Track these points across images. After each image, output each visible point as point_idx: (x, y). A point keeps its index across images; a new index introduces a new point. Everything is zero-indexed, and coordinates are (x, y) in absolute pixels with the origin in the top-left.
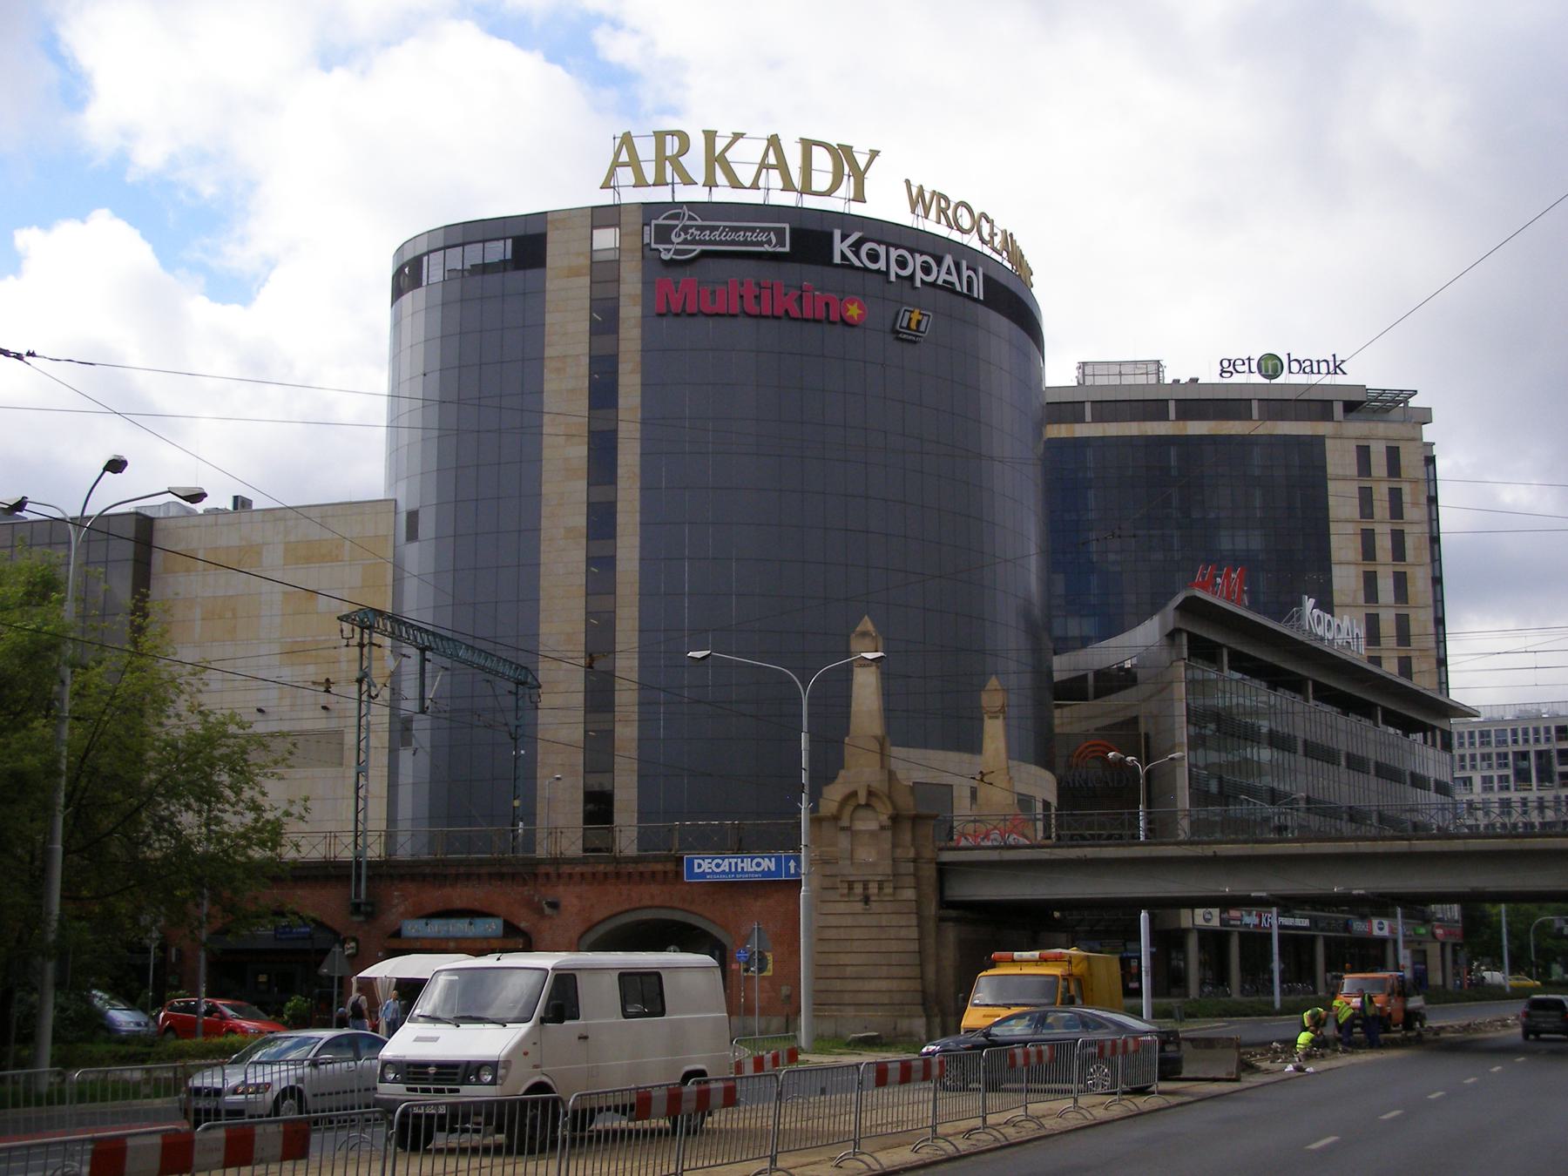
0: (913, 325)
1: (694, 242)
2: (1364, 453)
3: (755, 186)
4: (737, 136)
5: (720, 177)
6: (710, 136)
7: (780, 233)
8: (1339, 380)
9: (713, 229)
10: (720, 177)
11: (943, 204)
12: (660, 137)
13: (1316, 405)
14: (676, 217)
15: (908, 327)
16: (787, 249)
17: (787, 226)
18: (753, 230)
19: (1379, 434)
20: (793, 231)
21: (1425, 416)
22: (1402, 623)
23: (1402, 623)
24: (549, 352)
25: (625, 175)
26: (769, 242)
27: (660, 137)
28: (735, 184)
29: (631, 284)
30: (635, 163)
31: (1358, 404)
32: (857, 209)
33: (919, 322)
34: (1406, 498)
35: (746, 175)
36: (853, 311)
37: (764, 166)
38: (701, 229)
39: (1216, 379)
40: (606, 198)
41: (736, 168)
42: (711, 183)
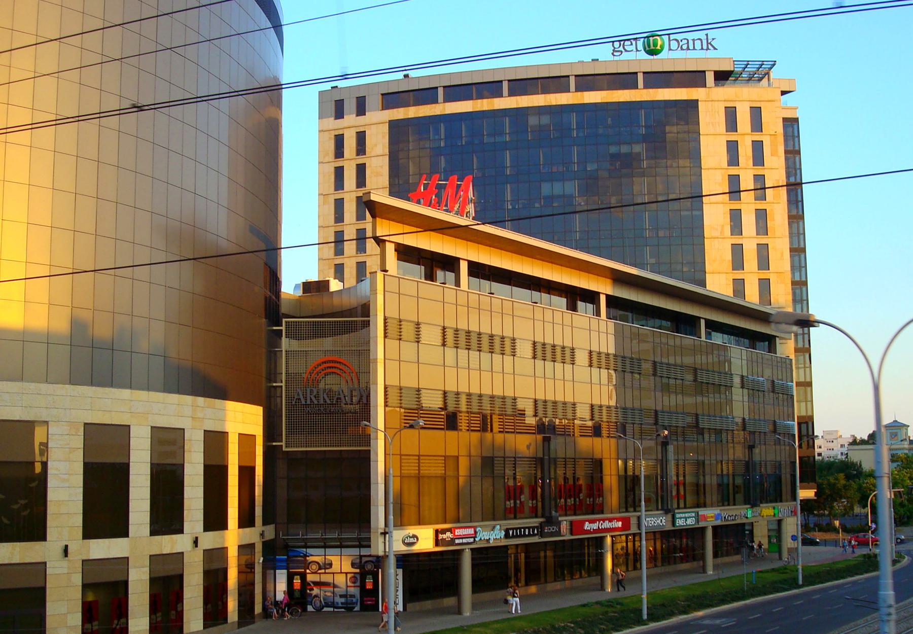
2: (731, 115)
16: (284, 320)
39: (611, 58)
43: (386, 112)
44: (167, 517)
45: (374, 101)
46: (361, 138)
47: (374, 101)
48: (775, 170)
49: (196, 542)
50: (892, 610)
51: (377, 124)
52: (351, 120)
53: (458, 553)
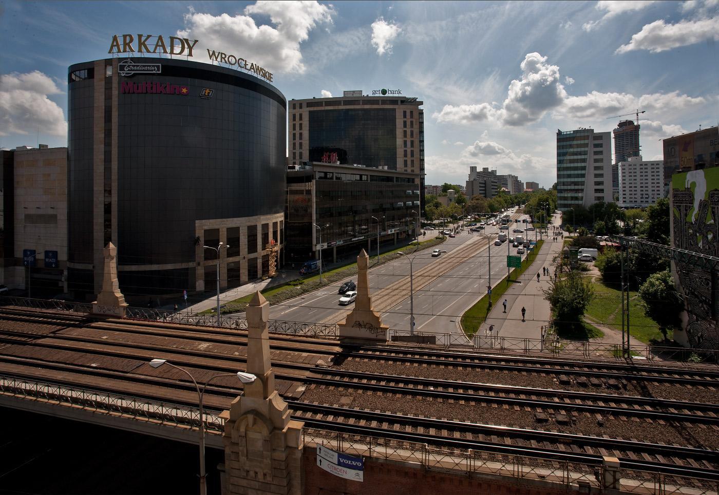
0: (206, 94)
1: (131, 70)
2: (405, 112)
3: (154, 52)
4: (149, 36)
5: (143, 49)
6: (140, 36)
7: (158, 67)
8: (400, 95)
9: (137, 66)
10: (143, 49)
11: (223, 56)
12: (125, 36)
13: (394, 101)
14: (126, 62)
15: (205, 95)
16: (160, 72)
17: (160, 65)
18: (150, 66)
19: (408, 108)
20: (162, 65)
21: (421, 103)
22: (412, 152)
23: (412, 152)
24: (95, 105)
25: (115, 49)
26: (155, 70)
27: (125, 36)
28: (148, 51)
29: (115, 84)
30: (118, 46)
31: (404, 101)
32: (190, 59)
33: (209, 93)
34: (414, 123)
35: (151, 49)
36: (184, 90)
37: (157, 45)
38: (134, 66)
39: (372, 95)
40: (110, 56)
41: (148, 46)
42: (140, 51)
43: (308, 108)
44: (252, 247)
45: (304, 105)
46: (301, 115)
47: (304, 105)
48: (416, 131)
49: (199, 264)
50: (614, 314)
51: (305, 112)
52: (298, 109)
53: (333, 248)
